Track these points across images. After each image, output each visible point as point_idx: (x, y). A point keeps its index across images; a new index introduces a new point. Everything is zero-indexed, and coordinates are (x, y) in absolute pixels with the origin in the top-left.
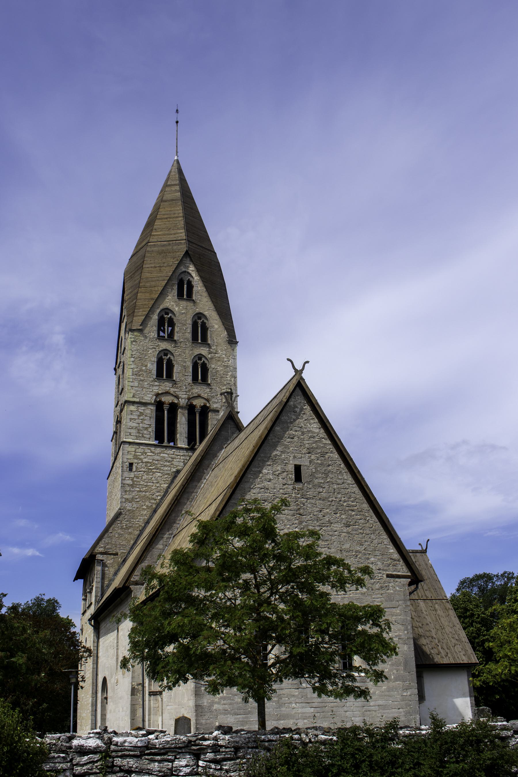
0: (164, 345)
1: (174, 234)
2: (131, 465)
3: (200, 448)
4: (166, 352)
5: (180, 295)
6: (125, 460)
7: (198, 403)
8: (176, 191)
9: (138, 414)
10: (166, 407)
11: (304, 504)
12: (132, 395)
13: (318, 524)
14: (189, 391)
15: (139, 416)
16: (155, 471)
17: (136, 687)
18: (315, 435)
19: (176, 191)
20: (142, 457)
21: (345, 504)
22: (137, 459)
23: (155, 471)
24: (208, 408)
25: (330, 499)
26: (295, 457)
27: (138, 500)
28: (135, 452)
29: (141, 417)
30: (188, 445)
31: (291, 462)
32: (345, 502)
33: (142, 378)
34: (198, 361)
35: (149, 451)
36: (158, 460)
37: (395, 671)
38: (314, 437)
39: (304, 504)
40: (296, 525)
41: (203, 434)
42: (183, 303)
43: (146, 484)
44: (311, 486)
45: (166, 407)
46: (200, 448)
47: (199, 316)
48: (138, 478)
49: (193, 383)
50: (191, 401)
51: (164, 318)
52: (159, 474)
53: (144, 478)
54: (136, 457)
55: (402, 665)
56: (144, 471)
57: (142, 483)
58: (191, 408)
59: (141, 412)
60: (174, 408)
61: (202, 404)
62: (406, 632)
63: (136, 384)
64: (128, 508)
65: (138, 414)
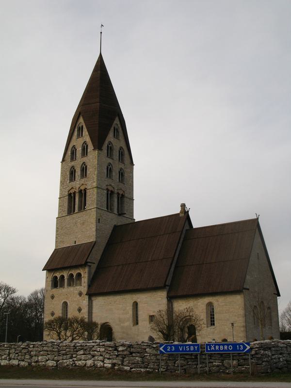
47: (85, 143)
60: (74, 193)
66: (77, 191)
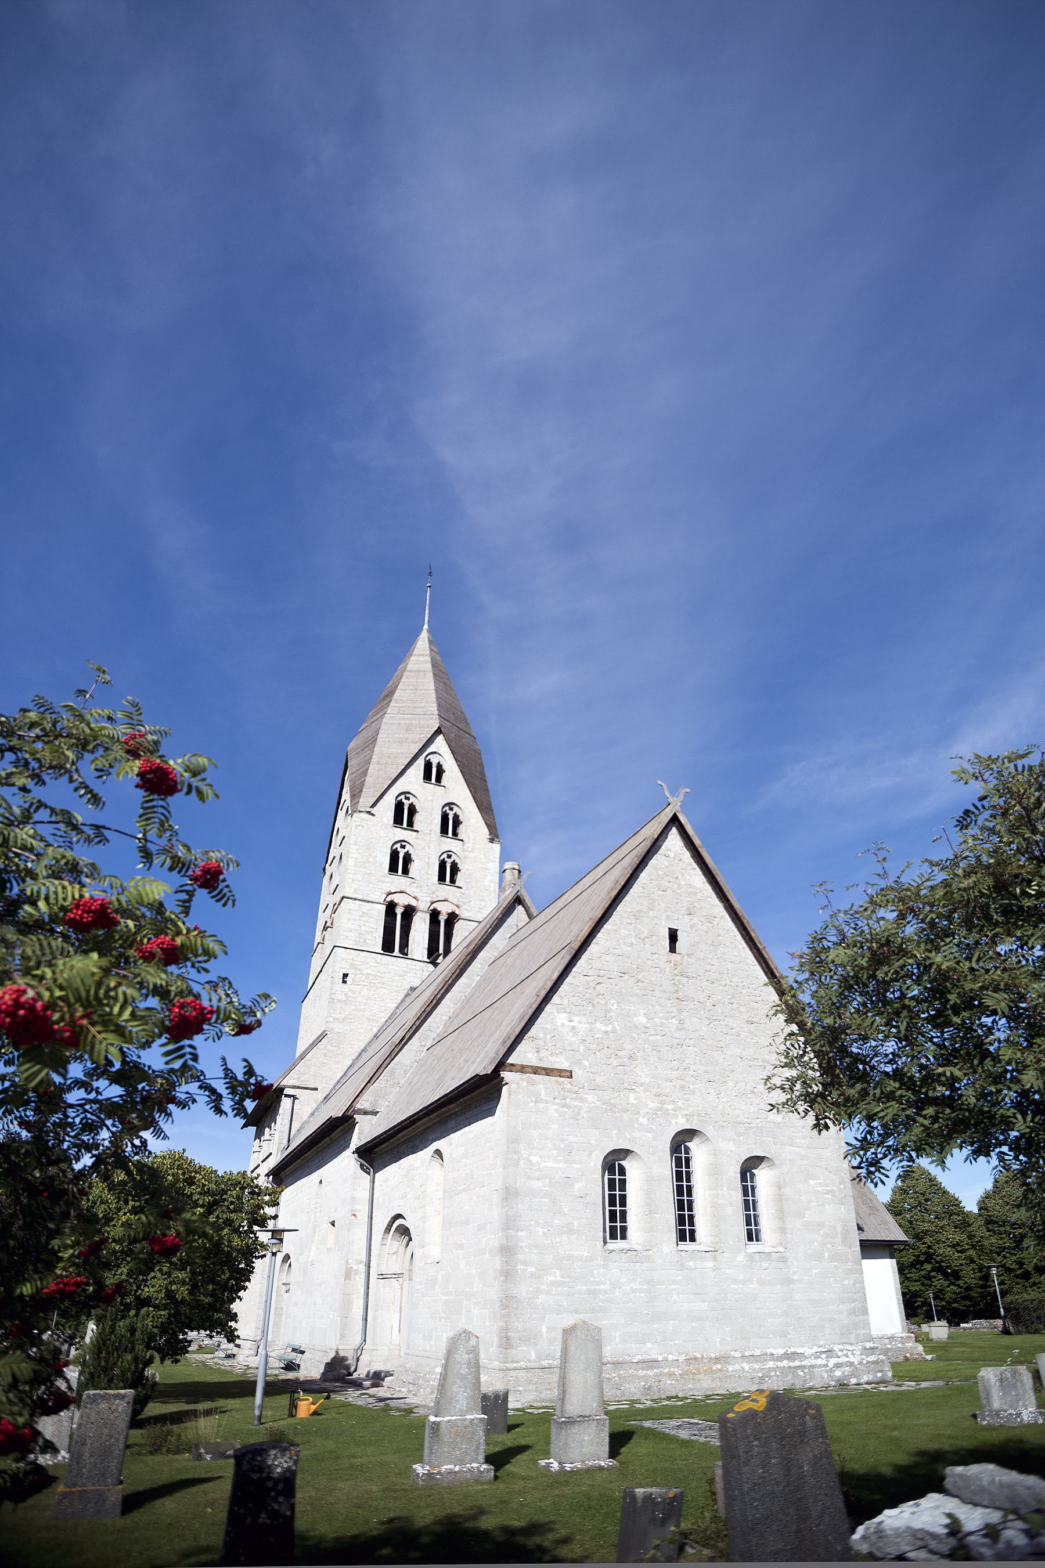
0: (401, 834)
1: (423, 707)
2: (345, 976)
3: (447, 964)
4: (403, 843)
5: (427, 777)
6: (337, 969)
7: (445, 909)
8: (426, 662)
9: (361, 914)
10: (399, 911)
11: (683, 985)
12: (353, 889)
13: (706, 1015)
14: (434, 893)
15: (361, 916)
16: (379, 985)
17: (355, 1267)
18: (698, 891)
19: (426, 662)
20: (362, 967)
21: (744, 991)
22: (355, 969)
23: (379, 985)
24: (457, 916)
25: (724, 983)
26: (668, 917)
27: (352, 1021)
28: (353, 960)
29: (365, 919)
30: (428, 958)
31: (663, 923)
32: (743, 987)
33: (368, 872)
34: (446, 859)
35: (373, 960)
36: (384, 973)
37: (829, 1246)
38: (695, 894)
39: (683, 985)
40: (673, 1015)
41: (447, 951)
42: (431, 788)
43: (365, 1001)
44: (693, 961)
45: (399, 911)
46: (447, 964)
48: (353, 992)
49: (279, 1186)
50: (435, 905)
51: (403, 804)
52: (385, 990)
53: (362, 993)
54: (353, 966)
55: (839, 1236)
56: (364, 986)
57: (360, 999)
58: (434, 915)
59: (363, 913)
60: (409, 912)
61: (450, 911)
62: (842, 1186)
63: (360, 877)
64: (337, 1030)
65: (361, 914)
66: (423, 905)
